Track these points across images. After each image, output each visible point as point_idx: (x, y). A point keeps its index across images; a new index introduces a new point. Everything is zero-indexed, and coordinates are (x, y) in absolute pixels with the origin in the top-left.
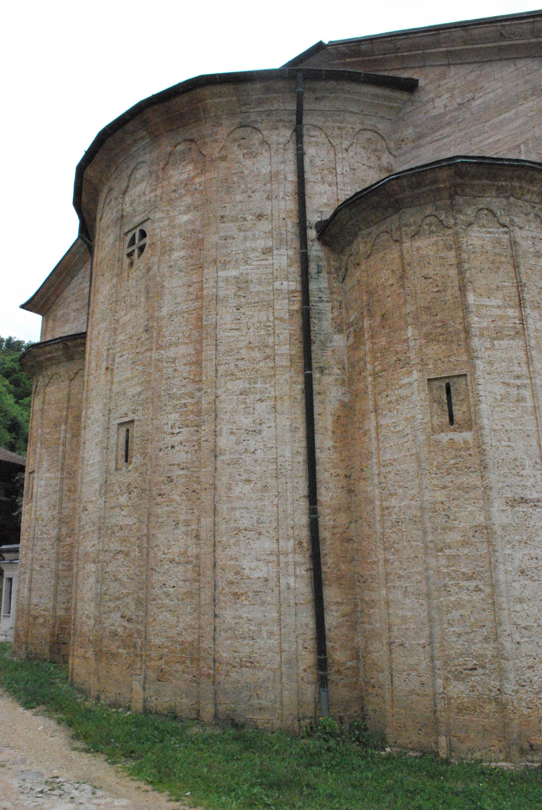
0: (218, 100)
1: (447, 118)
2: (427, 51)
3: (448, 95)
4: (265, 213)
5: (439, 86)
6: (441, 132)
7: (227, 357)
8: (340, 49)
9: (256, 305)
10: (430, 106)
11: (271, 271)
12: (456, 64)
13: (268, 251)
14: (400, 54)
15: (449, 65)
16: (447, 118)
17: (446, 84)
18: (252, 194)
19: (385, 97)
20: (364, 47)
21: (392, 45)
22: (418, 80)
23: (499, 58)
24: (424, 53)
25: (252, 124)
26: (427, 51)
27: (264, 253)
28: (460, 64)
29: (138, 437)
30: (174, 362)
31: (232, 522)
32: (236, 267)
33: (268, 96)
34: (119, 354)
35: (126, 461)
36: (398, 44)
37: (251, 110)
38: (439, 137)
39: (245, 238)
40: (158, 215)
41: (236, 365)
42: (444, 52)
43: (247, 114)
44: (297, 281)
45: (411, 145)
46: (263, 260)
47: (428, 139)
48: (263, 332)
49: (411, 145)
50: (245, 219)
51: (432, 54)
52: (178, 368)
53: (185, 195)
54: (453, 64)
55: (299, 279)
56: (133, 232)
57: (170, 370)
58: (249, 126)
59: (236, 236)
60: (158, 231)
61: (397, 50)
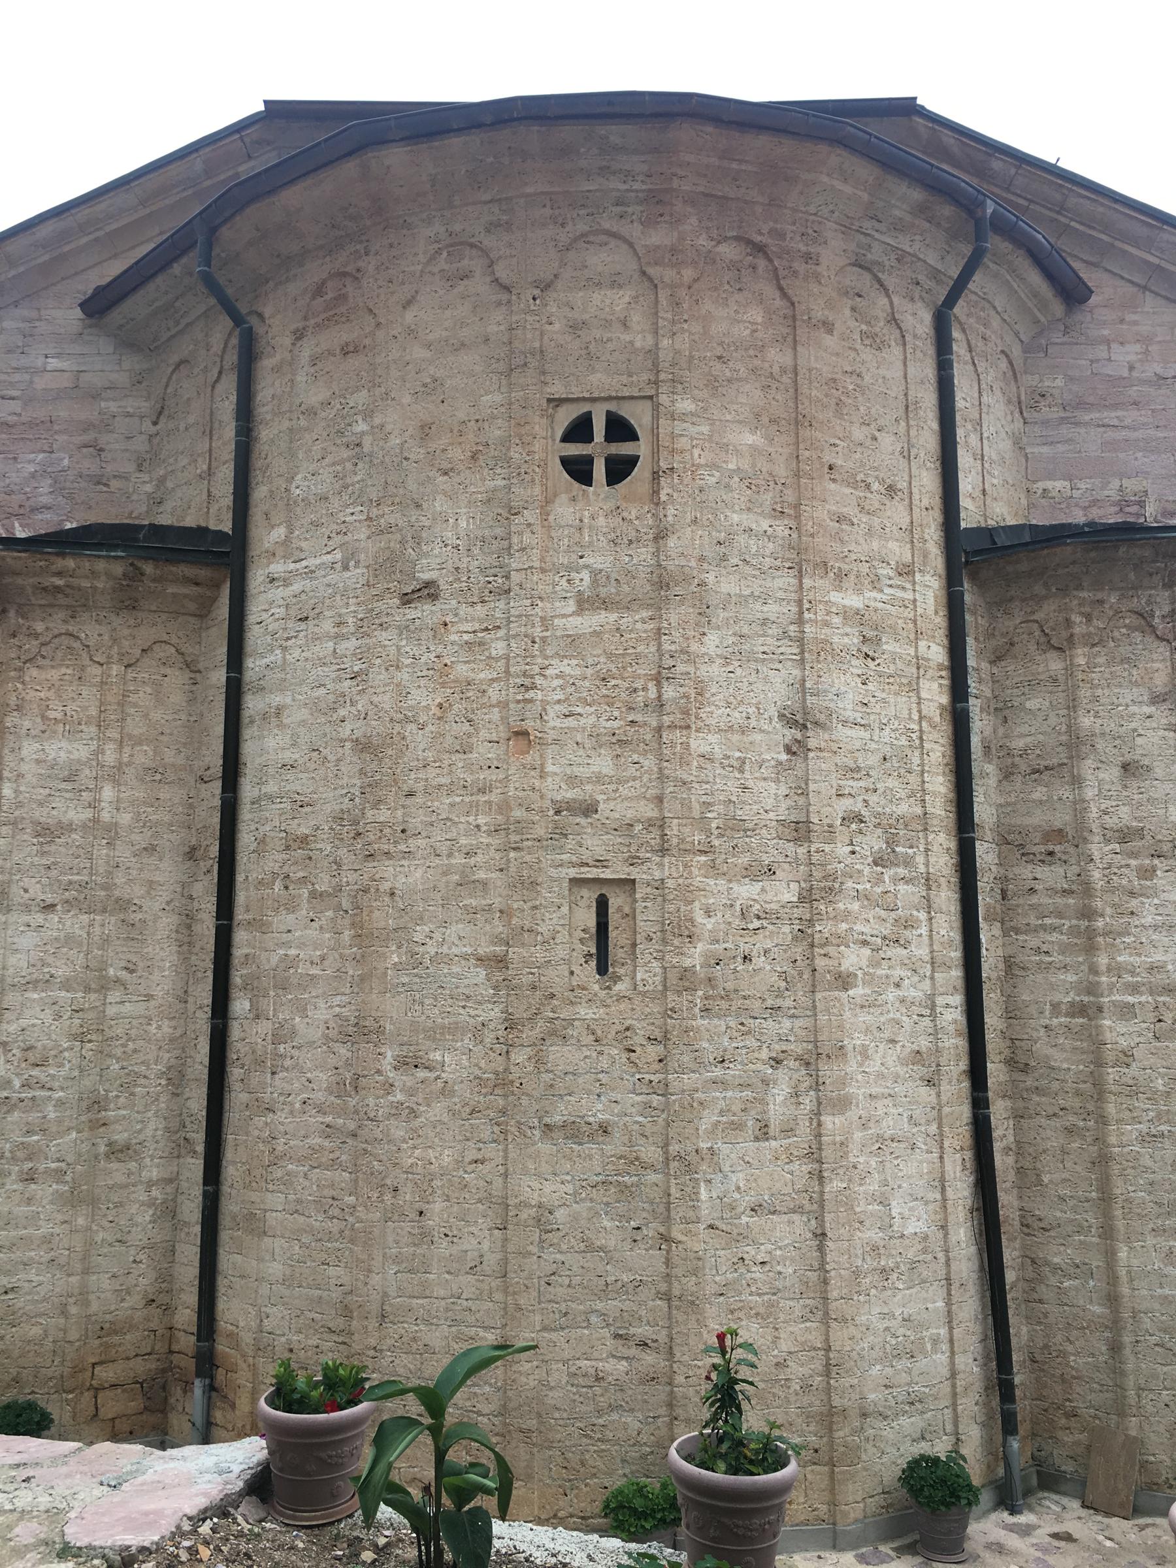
0: (839, 185)
1: (1133, 392)
2: (1118, 244)
3: (1138, 348)
4: (899, 487)
5: (1122, 321)
6: (1120, 413)
7: (851, 783)
8: (945, 139)
9: (891, 680)
10: (1101, 352)
11: (911, 616)
12: (1157, 294)
13: (906, 571)
14: (1063, 219)
15: (1145, 288)
16: (1133, 392)
17: (1135, 323)
18: (877, 434)
19: (1035, 295)
20: (997, 165)
21: (1058, 197)
22: (1092, 292)
23: (1143, 283)
24: (1113, 245)
25: (875, 269)
26: (1118, 244)
27: (900, 574)
28: (1167, 299)
29: (1046, 978)
30: (742, 771)
31: (871, 1124)
32: (859, 592)
33: (917, 222)
34: (563, 709)
35: (602, 969)
36: (1072, 201)
37: (877, 235)
38: (1115, 422)
39: (870, 532)
40: (685, 405)
41: (865, 801)
42: (1153, 264)
43: (868, 240)
44: (944, 647)
45: (1056, 413)
46: (898, 587)
47: (1095, 415)
48: (903, 741)
49: (1056, 413)
50: (868, 486)
51: (1125, 252)
52: (750, 783)
53: (746, 380)
54: (1152, 292)
55: (946, 642)
56: (584, 408)
57: (732, 786)
58: (868, 269)
59: (855, 521)
60: (683, 443)
61: (1061, 209)
